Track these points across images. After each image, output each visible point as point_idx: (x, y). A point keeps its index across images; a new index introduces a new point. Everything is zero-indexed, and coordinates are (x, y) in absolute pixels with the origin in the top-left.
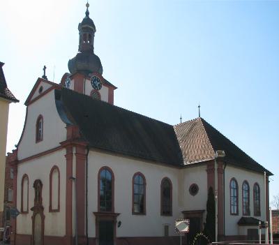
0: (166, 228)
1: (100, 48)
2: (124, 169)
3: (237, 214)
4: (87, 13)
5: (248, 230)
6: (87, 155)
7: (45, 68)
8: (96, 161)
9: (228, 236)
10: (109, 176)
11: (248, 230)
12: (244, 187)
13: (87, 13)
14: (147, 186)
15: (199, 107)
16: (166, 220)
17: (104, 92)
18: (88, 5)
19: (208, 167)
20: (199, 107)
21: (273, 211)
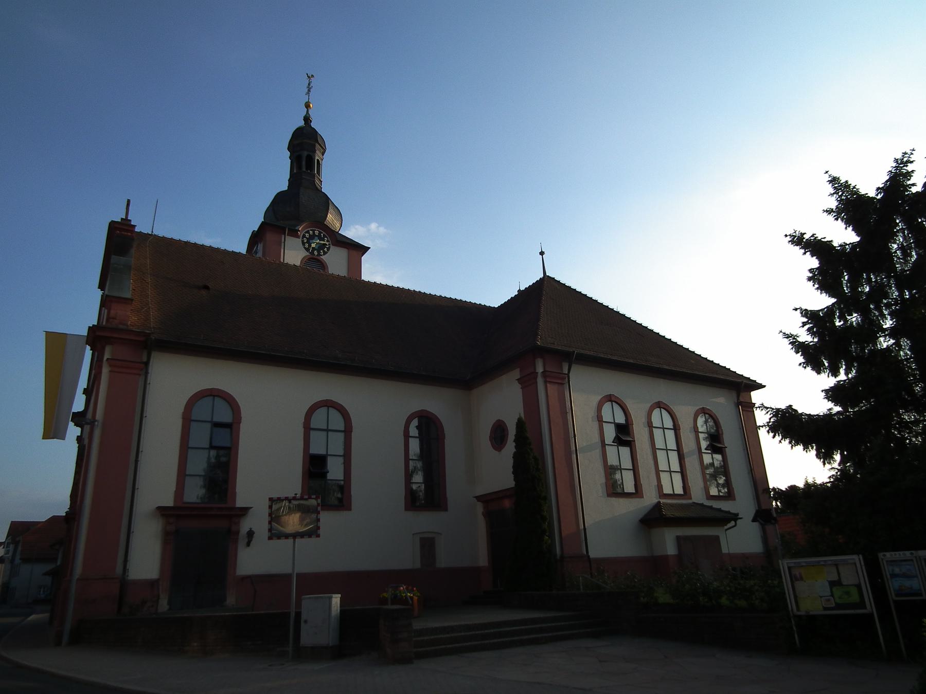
0: (428, 545)
1: (331, 181)
2: (274, 408)
3: (638, 492)
4: (307, 119)
5: (678, 538)
6: (147, 364)
7: (129, 201)
8: (174, 382)
9: (600, 561)
10: (224, 415)
11: (678, 538)
12: (656, 421)
13: (307, 119)
14: (354, 435)
15: (542, 253)
16: (426, 521)
17: (336, 262)
18: (307, 106)
19: (521, 371)
20: (542, 253)
21: (717, 538)
